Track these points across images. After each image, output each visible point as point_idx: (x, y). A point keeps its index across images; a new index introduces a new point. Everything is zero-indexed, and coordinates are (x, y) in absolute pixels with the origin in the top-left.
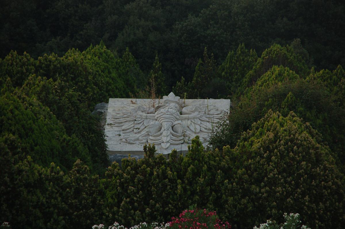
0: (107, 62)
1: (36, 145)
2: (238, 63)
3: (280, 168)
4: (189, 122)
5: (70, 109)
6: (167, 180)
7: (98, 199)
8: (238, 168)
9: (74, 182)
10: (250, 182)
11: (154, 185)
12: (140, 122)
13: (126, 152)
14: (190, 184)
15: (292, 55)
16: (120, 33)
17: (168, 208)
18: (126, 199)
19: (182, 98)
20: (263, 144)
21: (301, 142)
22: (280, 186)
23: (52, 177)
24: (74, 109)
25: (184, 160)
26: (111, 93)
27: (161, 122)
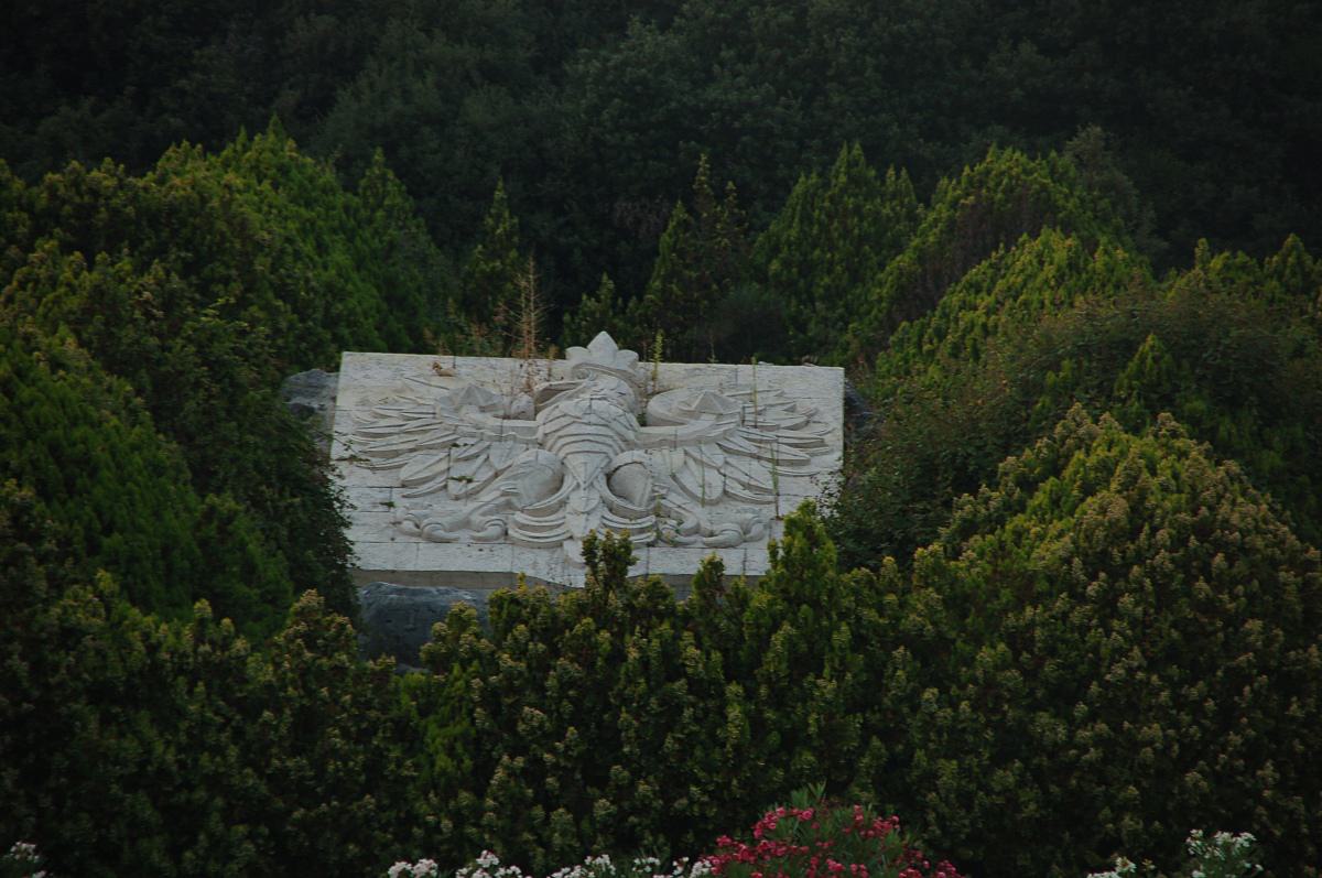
0: (308, 205)
1: (108, 530)
2: (836, 224)
3: (1153, 644)
4: (677, 457)
5: (206, 390)
6: (683, 681)
7: (392, 755)
8: (977, 640)
9: (293, 682)
10: (1029, 700)
11: (626, 701)
12: (473, 451)
13: (417, 574)
14: (779, 700)
15: (1071, 194)
16: (345, 89)
17: (684, 801)
18: (512, 757)
19: (645, 356)
20: (1083, 544)
21: (1243, 537)
22: (1157, 719)
23: (200, 658)
24: (222, 389)
25: (754, 604)
26: (345, 332)
27: (561, 455)
